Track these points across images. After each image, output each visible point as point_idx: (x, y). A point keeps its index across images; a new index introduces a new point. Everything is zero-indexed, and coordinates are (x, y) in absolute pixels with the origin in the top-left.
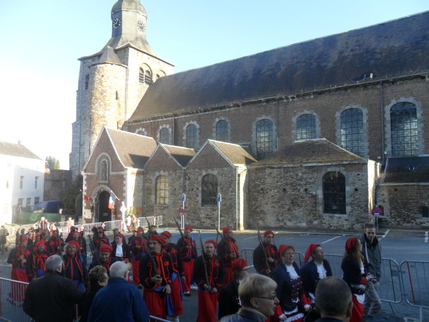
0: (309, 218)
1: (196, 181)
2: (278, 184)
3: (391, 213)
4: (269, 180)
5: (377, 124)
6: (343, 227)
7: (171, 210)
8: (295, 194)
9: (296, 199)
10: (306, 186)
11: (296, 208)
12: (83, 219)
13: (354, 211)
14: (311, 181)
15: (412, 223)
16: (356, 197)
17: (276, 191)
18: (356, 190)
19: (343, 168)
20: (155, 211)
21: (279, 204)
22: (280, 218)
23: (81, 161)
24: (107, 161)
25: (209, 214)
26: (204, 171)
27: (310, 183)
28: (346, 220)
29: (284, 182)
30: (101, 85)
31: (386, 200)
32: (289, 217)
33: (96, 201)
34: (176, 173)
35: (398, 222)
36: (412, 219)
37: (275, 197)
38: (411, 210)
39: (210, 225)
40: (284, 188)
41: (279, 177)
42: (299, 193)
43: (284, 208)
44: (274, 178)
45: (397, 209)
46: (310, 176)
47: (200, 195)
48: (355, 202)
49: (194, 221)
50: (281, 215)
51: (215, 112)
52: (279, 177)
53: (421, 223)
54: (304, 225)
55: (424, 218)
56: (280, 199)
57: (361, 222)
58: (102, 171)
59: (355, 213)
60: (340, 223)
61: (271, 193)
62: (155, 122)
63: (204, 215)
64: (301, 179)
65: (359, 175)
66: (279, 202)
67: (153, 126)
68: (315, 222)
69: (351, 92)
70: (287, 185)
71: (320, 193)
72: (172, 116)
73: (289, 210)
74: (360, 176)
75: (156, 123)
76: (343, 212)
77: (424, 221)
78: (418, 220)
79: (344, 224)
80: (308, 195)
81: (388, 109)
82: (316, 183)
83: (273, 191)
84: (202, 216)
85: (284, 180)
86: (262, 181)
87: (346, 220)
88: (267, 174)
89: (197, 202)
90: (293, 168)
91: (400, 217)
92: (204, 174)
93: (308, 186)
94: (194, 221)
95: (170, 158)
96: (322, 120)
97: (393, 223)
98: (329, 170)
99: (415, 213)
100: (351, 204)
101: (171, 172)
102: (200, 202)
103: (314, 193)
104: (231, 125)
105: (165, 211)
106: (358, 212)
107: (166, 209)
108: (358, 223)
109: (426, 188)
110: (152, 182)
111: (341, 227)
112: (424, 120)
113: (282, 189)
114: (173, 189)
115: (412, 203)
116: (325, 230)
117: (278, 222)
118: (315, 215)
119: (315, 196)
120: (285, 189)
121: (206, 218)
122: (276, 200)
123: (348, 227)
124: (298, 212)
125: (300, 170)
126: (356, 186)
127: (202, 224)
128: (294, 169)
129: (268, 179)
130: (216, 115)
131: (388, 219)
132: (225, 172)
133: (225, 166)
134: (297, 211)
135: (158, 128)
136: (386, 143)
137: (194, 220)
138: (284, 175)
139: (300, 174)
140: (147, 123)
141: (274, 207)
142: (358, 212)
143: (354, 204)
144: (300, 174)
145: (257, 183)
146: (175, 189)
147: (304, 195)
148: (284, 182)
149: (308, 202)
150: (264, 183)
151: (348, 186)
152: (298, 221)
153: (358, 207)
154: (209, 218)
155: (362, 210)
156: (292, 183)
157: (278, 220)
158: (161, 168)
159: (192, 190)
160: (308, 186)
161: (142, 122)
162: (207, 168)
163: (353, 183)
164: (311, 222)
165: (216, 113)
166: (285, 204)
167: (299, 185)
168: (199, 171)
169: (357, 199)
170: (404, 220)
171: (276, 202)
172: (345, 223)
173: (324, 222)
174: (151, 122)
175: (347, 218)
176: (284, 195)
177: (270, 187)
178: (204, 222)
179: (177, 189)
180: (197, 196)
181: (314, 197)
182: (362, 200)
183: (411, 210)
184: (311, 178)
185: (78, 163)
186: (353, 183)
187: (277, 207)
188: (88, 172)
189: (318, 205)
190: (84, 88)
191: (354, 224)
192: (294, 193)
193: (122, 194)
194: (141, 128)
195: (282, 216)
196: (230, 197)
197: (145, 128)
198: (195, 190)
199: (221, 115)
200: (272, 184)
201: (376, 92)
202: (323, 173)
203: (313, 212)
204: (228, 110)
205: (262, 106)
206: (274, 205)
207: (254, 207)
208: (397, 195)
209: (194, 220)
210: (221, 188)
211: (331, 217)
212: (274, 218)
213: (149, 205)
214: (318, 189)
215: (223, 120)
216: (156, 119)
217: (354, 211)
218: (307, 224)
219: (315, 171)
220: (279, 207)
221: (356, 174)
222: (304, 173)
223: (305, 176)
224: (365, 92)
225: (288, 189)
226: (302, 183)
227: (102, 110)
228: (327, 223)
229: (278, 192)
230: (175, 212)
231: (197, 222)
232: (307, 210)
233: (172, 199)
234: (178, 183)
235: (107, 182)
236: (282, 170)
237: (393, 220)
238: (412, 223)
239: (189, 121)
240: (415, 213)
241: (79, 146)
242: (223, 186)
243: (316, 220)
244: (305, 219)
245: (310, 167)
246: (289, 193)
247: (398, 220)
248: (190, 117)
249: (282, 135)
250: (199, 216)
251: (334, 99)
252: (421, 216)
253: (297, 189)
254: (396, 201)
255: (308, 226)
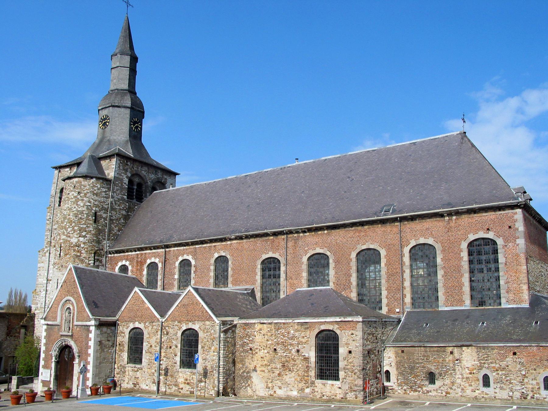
0: (301, 385)
1: (174, 337)
2: (269, 343)
3: (398, 380)
4: (258, 338)
5: (396, 269)
6: (336, 396)
7: (146, 373)
8: (286, 356)
9: (287, 361)
10: (298, 347)
11: (287, 373)
12: (40, 381)
13: (347, 378)
14: (304, 340)
15: (419, 391)
16: (350, 361)
17: (266, 351)
18: (350, 352)
19: (337, 326)
20: (127, 373)
21: (269, 368)
22: (270, 385)
23: (47, 302)
24: (71, 308)
25: (188, 378)
26: (184, 325)
27: (302, 343)
28: (340, 388)
29: (275, 340)
30: (77, 205)
31: (393, 364)
32: (280, 384)
33: (56, 359)
34: (153, 326)
35: (405, 390)
36: (419, 387)
37: (265, 358)
38: (418, 376)
39: (189, 392)
40: (275, 347)
41: (269, 334)
42: (290, 355)
43: (273, 373)
44: (264, 335)
45: (403, 374)
46: (303, 334)
47: (179, 354)
48: (349, 367)
49: (171, 387)
50: (270, 381)
51: (214, 244)
52: (269, 334)
53: (428, 392)
54: (295, 393)
55: (430, 386)
56: (271, 361)
57: (354, 391)
58: (65, 320)
59: (349, 379)
60: (333, 392)
61: (261, 353)
62: (142, 254)
63: (183, 380)
64: (292, 338)
65: (352, 334)
66: (269, 365)
67: (139, 260)
68: (307, 391)
69: (369, 228)
70: (278, 344)
71: (312, 355)
72: (162, 248)
73: (279, 375)
74: (354, 335)
75: (143, 256)
76: (336, 378)
77: (431, 389)
78: (424, 389)
79: (337, 392)
80: (300, 357)
81: (406, 250)
82: (309, 342)
83: (263, 351)
84: (181, 380)
85: (275, 338)
86: (251, 339)
87: (340, 388)
88: (257, 330)
89: (176, 363)
90: (284, 323)
91: (407, 384)
92: (184, 328)
93: (300, 346)
94: (171, 387)
95: (146, 306)
96: (337, 262)
97: (399, 391)
98: (323, 327)
99: (422, 380)
100: (344, 368)
101: (147, 324)
102: (178, 363)
103: (307, 355)
104: (232, 263)
105: (138, 373)
106: (351, 378)
107: (140, 371)
108: (351, 391)
109: (432, 350)
110: (125, 336)
111: (334, 397)
112: (444, 267)
113: (273, 350)
114: (149, 345)
115: (419, 367)
116: (317, 400)
117: (267, 390)
118: (306, 382)
119: (307, 358)
120: (275, 349)
121: (185, 383)
122: (266, 362)
123: (341, 396)
124: (290, 377)
125: (292, 326)
126: (349, 347)
127: (180, 390)
128: (286, 326)
129: (257, 337)
130: (216, 250)
131: (395, 387)
132: (207, 327)
133: (208, 320)
134: (288, 376)
135: (145, 262)
136: (405, 293)
137: (171, 385)
138: (275, 332)
139: (292, 332)
140: (132, 255)
141: (264, 371)
142: (351, 378)
143: (347, 369)
144: (292, 332)
145: (246, 341)
146: (151, 346)
147: (296, 357)
148: (275, 340)
149: (300, 365)
150: (252, 341)
151: (341, 347)
152: (288, 389)
153: (352, 372)
154: (188, 384)
155: (356, 377)
156: (282, 342)
157: (268, 387)
158: (136, 319)
159: (170, 347)
160: (300, 346)
161: (127, 254)
162: (188, 321)
163: (346, 344)
164: (302, 390)
165: (214, 246)
166: (275, 368)
167: (291, 345)
168: (179, 324)
169: (351, 363)
170: (411, 388)
171: (266, 365)
172: (339, 391)
173: (316, 390)
174: (138, 254)
175: (340, 386)
176: (274, 357)
177: (260, 346)
178: (182, 389)
179: (153, 346)
180: (176, 355)
181: (306, 359)
182: (356, 365)
183: (418, 376)
184: (303, 337)
185: (44, 304)
186: (346, 344)
187: (266, 371)
188: (49, 321)
189: (310, 369)
190: (57, 205)
191: (348, 393)
192: (285, 354)
193: (87, 351)
194: (124, 261)
195: (272, 382)
196: (212, 357)
197: (130, 261)
198: (173, 347)
199: (222, 249)
200: (262, 342)
201: (395, 230)
202: (317, 331)
203: (304, 379)
204: (229, 243)
205: (269, 239)
206: (263, 369)
207: (242, 371)
208: (404, 357)
209: (171, 385)
210: (202, 347)
211: (324, 384)
212: (263, 385)
213: (121, 365)
214: (310, 350)
215: (223, 256)
216: (143, 250)
217: (347, 378)
218: (298, 392)
219: (308, 328)
220: (269, 372)
221: (350, 333)
222: (296, 330)
223: (297, 334)
224: (383, 229)
225: (278, 350)
226: (294, 343)
227: (76, 236)
228: (319, 391)
229: (268, 352)
230: (150, 375)
231: (174, 388)
232: (299, 376)
233: (147, 358)
234: (154, 338)
235: (70, 334)
236: (273, 326)
237: (400, 388)
238: (419, 391)
239: (183, 255)
240: (422, 380)
241: (46, 281)
242: (205, 344)
243: (307, 387)
244: (296, 386)
245: (302, 324)
246: (279, 354)
247: (405, 388)
248: (184, 249)
249: (291, 278)
250: (176, 381)
251: (349, 235)
252: (427, 383)
253: (288, 349)
254: (402, 365)
255: (299, 395)
